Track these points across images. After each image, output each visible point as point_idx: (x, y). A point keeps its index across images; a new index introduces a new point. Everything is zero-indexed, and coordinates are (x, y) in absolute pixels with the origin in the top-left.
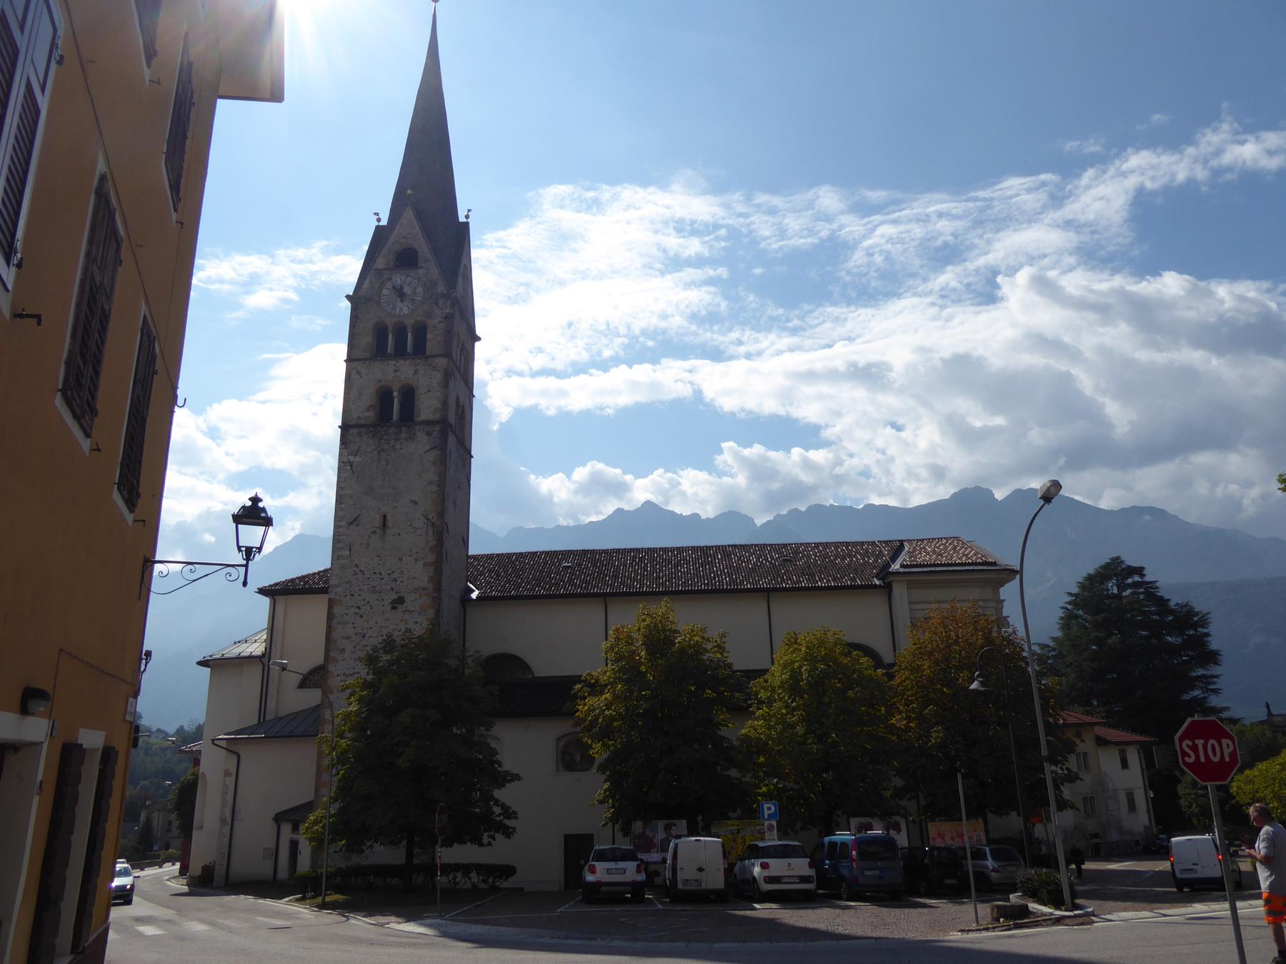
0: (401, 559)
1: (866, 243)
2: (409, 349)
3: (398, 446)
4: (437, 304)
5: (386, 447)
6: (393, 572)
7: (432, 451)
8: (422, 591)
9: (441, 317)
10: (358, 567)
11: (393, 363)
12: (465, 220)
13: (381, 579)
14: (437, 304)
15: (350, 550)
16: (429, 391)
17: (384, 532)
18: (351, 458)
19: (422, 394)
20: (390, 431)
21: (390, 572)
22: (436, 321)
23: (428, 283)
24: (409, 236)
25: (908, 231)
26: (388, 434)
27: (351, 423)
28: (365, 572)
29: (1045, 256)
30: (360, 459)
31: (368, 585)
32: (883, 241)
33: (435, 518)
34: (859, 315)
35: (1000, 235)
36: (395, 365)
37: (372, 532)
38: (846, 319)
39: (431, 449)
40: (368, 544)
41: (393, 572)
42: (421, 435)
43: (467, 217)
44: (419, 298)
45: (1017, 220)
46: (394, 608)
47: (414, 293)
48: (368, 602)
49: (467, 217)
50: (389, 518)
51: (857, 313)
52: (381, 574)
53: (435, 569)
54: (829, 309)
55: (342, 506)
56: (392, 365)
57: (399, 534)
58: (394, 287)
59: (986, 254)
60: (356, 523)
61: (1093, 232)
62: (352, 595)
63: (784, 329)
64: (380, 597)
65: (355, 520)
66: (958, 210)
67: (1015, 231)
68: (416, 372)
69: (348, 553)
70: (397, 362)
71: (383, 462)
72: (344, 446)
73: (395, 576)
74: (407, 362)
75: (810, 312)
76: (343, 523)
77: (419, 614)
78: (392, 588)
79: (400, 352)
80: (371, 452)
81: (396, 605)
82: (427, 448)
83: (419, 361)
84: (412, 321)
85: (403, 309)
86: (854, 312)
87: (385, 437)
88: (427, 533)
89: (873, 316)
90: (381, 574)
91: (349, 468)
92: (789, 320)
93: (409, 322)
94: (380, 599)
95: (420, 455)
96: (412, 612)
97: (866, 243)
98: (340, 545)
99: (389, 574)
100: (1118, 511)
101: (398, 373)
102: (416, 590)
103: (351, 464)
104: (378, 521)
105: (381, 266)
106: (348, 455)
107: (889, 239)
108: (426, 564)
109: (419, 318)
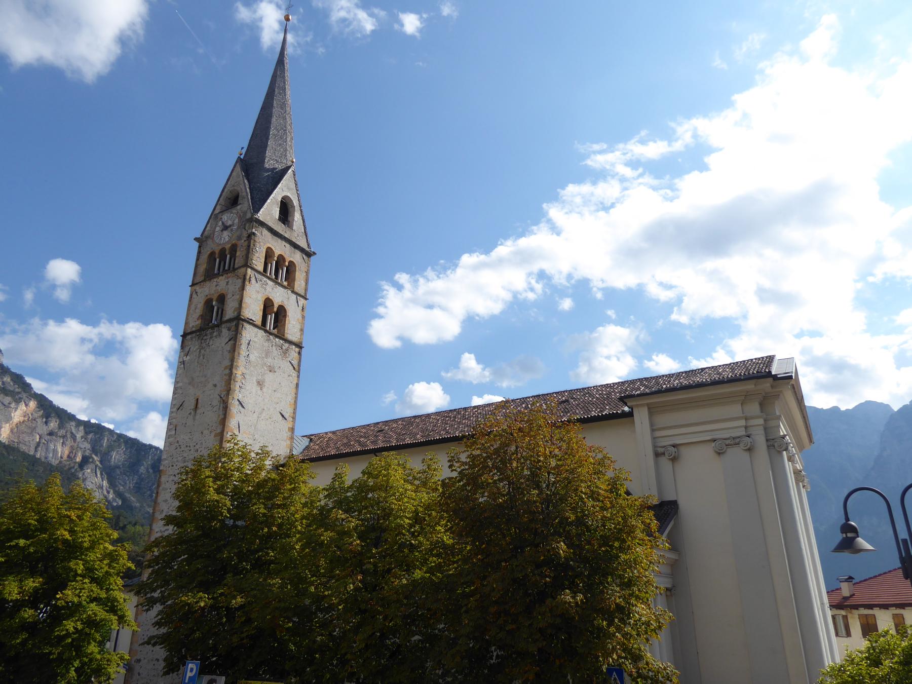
0: (202, 433)
73: (197, 447)
109: (234, 242)
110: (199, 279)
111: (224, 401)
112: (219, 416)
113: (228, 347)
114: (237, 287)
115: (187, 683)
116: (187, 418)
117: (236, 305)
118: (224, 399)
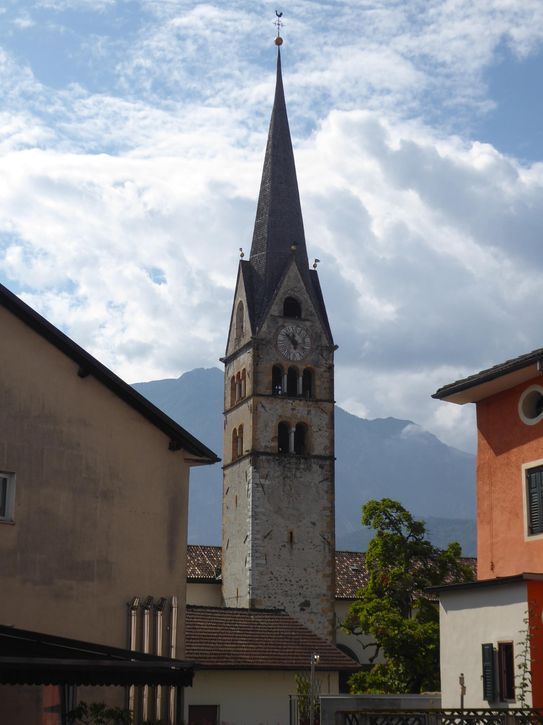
0: (305, 570)
1: (178, 21)
2: (300, 391)
3: (298, 474)
4: (322, 355)
5: (289, 474)
6: (300, 580)
7: (324, 482)
8: (323, 597)
9: (326, 368)
10: (273, 574)
11: (291, 402)
12: (313, 269)
13: (291, 585)
14: (322, 355)
15: (266, 559)
16: (320, 430)
17: (292, 546)
18: (263, 481)
19: (314, 432)
20: (292, 461)
21: (298, 580)
22: (322, 370)
23: (313, 335)
24: (295, 289)
25: (235, 20)
26: (289, 463)
27: (260, 451)
28: (279, 578)
29: (388, 91)
30: (269, 483)
31: (282, 589)
32: (200, 24)
33: (330, 538)
34: (144, 118)
35: (343, 50)
36: (292, 404)
37: (282, 546)
38: (127, 118)
39: (324, 480)
40: (280, 555)
41: (300, 580)
42: (315, 467)
43: (315, 266)
44: (308, 348)
45: (368, 37)
46: (302, 610)
47: (304, 342)
48: (282, 604)
49: (315, 266)
50: (295, 535)
51: (141, 114)
52: (291, 581)
53: (331, 579)
54: (108, 100)
55: (258, 521)
56: (289, 403)
57: (303, 549)
58: (288, 335)
59: (322, 70)
60: (269, 537)
61: (448, 76)
62: (270, 597)
63: (37, 113)
64: (291, 600)
65: (268, 534)
66: (300, 9)
67: (363, 49)
68: (309, 412)
69: (264, 562)
70: (294, 402)
71: (288, 487)
72: (256, 470)
73: (302, 583)
74: (302, 403)
75: (81, 97)
76: (259, 536)
77: (322, 615)
78: (300, 593)
79: (292, 393)
80: (278, 477)
81: (304, 608)
82: (321, 478)
83: (311, 403)
84: (304, 367)
85: (296, 355)
86: (139, 110)
87: (288, 466)
88: (324, 550)
89: (164, 123)
90: (291, 581)
91: (261, 489)
92: (49, 102)
93: (301, 368)
94: (291, 601)
95: (316, 484)
96: (316, 614)
97: (178, 21)
98: (258, 555)
99: (297, 582)
100: (360, 419)
101: (295, 412)
102: (318, 596)
103: (263, 486)
104: (286, 537)
105: (276, 313)
106: (259, 478)
107: (209, 24)
108: (324, 576)
109: (309, 366)
110: (228, 406)
111: (329, 543)
112: (325, 557)
113: (325, 486)
114: (324, 423)
115: (488, 722)
116: (280, 550)
117: (327, 442)
118: (329, 540)
